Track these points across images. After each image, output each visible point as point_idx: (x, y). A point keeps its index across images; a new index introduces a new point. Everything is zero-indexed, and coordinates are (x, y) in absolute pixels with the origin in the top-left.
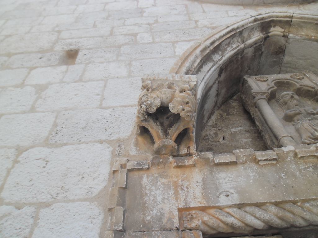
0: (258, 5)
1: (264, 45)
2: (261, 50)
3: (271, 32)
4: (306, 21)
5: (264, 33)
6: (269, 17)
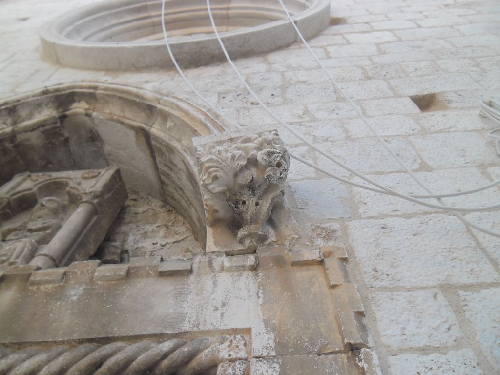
0: (97, 70)
1: (63, 127)
2: (62, 135)
3: (71, 109)
4: (111, 93)
5: (61, 110)
6: (69, 88)
